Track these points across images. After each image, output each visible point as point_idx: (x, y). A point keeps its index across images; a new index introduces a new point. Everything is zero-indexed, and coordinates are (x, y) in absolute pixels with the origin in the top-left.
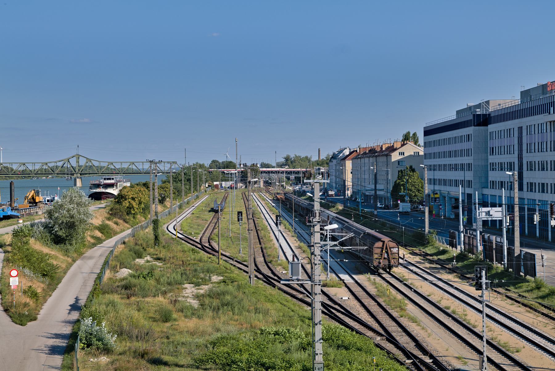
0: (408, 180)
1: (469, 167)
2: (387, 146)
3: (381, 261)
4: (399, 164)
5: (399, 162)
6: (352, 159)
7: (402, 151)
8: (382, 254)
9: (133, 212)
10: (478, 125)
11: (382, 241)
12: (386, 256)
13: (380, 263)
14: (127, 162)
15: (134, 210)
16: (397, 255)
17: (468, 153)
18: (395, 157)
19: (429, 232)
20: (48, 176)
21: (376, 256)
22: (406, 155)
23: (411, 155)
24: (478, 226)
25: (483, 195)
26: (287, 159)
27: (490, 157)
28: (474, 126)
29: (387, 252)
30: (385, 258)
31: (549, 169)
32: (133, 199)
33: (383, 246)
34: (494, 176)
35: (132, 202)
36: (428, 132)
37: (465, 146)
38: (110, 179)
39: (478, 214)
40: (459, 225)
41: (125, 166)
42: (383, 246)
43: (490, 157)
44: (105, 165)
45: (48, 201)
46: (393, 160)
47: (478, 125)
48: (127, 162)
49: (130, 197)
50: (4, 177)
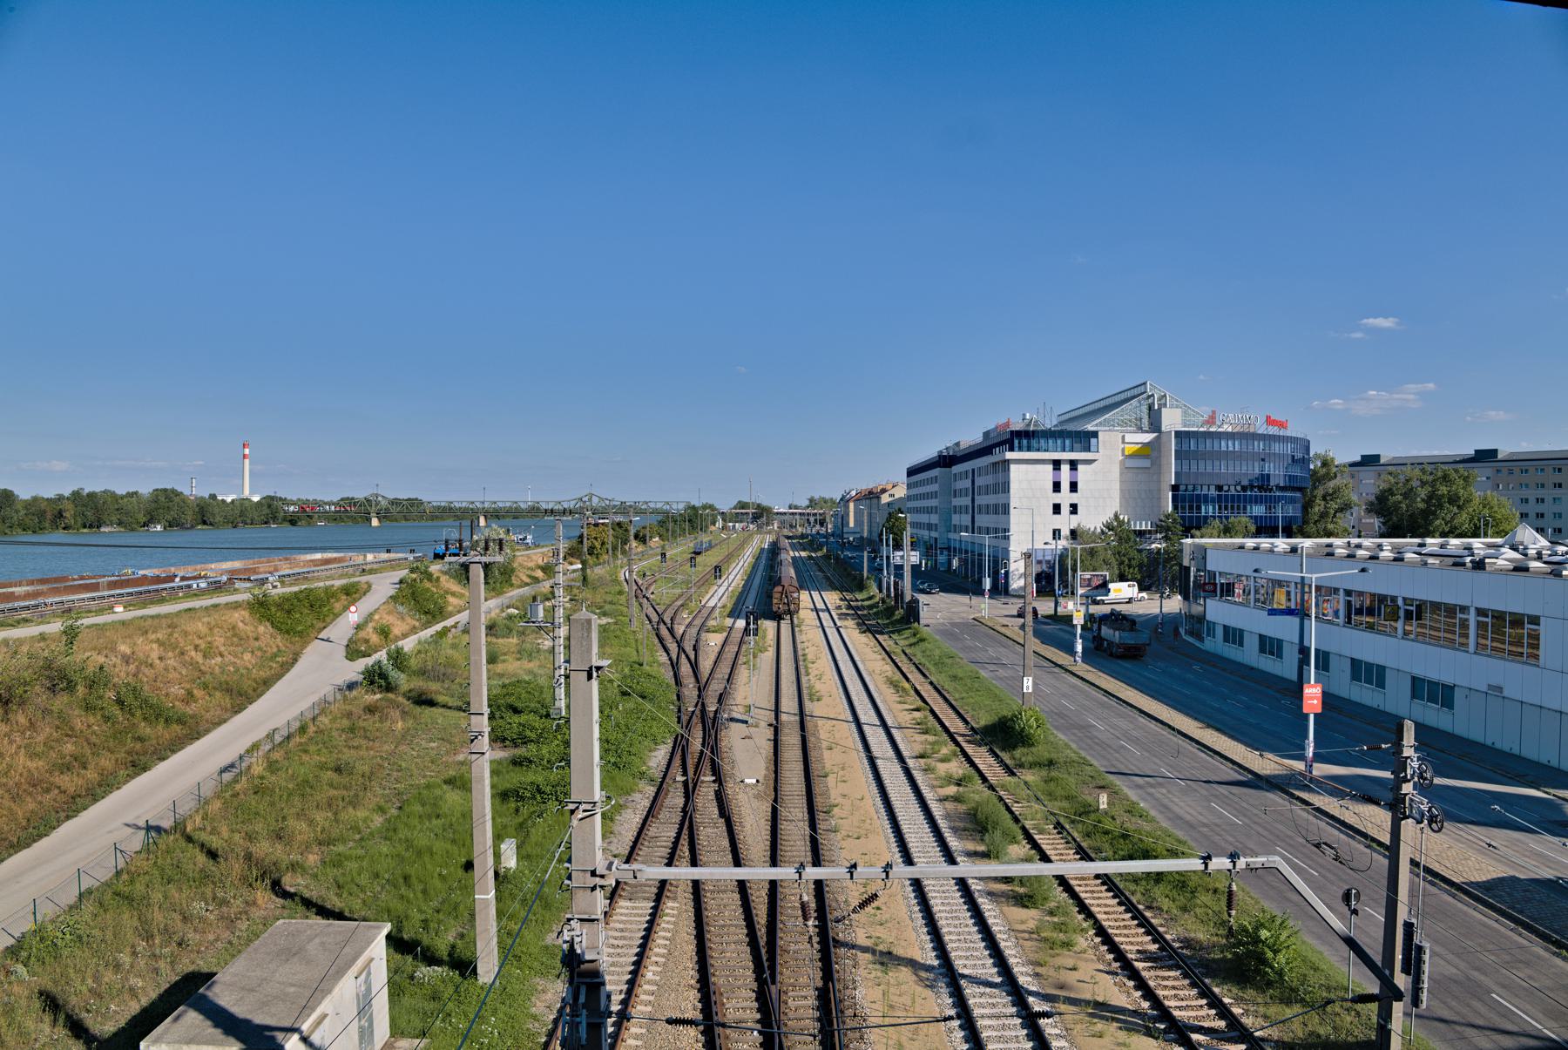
17: (934, 495)
18: (885, 499)
34: (956, 519)
36: (911, 472)
37: (934, 487)
41: (659, 506)
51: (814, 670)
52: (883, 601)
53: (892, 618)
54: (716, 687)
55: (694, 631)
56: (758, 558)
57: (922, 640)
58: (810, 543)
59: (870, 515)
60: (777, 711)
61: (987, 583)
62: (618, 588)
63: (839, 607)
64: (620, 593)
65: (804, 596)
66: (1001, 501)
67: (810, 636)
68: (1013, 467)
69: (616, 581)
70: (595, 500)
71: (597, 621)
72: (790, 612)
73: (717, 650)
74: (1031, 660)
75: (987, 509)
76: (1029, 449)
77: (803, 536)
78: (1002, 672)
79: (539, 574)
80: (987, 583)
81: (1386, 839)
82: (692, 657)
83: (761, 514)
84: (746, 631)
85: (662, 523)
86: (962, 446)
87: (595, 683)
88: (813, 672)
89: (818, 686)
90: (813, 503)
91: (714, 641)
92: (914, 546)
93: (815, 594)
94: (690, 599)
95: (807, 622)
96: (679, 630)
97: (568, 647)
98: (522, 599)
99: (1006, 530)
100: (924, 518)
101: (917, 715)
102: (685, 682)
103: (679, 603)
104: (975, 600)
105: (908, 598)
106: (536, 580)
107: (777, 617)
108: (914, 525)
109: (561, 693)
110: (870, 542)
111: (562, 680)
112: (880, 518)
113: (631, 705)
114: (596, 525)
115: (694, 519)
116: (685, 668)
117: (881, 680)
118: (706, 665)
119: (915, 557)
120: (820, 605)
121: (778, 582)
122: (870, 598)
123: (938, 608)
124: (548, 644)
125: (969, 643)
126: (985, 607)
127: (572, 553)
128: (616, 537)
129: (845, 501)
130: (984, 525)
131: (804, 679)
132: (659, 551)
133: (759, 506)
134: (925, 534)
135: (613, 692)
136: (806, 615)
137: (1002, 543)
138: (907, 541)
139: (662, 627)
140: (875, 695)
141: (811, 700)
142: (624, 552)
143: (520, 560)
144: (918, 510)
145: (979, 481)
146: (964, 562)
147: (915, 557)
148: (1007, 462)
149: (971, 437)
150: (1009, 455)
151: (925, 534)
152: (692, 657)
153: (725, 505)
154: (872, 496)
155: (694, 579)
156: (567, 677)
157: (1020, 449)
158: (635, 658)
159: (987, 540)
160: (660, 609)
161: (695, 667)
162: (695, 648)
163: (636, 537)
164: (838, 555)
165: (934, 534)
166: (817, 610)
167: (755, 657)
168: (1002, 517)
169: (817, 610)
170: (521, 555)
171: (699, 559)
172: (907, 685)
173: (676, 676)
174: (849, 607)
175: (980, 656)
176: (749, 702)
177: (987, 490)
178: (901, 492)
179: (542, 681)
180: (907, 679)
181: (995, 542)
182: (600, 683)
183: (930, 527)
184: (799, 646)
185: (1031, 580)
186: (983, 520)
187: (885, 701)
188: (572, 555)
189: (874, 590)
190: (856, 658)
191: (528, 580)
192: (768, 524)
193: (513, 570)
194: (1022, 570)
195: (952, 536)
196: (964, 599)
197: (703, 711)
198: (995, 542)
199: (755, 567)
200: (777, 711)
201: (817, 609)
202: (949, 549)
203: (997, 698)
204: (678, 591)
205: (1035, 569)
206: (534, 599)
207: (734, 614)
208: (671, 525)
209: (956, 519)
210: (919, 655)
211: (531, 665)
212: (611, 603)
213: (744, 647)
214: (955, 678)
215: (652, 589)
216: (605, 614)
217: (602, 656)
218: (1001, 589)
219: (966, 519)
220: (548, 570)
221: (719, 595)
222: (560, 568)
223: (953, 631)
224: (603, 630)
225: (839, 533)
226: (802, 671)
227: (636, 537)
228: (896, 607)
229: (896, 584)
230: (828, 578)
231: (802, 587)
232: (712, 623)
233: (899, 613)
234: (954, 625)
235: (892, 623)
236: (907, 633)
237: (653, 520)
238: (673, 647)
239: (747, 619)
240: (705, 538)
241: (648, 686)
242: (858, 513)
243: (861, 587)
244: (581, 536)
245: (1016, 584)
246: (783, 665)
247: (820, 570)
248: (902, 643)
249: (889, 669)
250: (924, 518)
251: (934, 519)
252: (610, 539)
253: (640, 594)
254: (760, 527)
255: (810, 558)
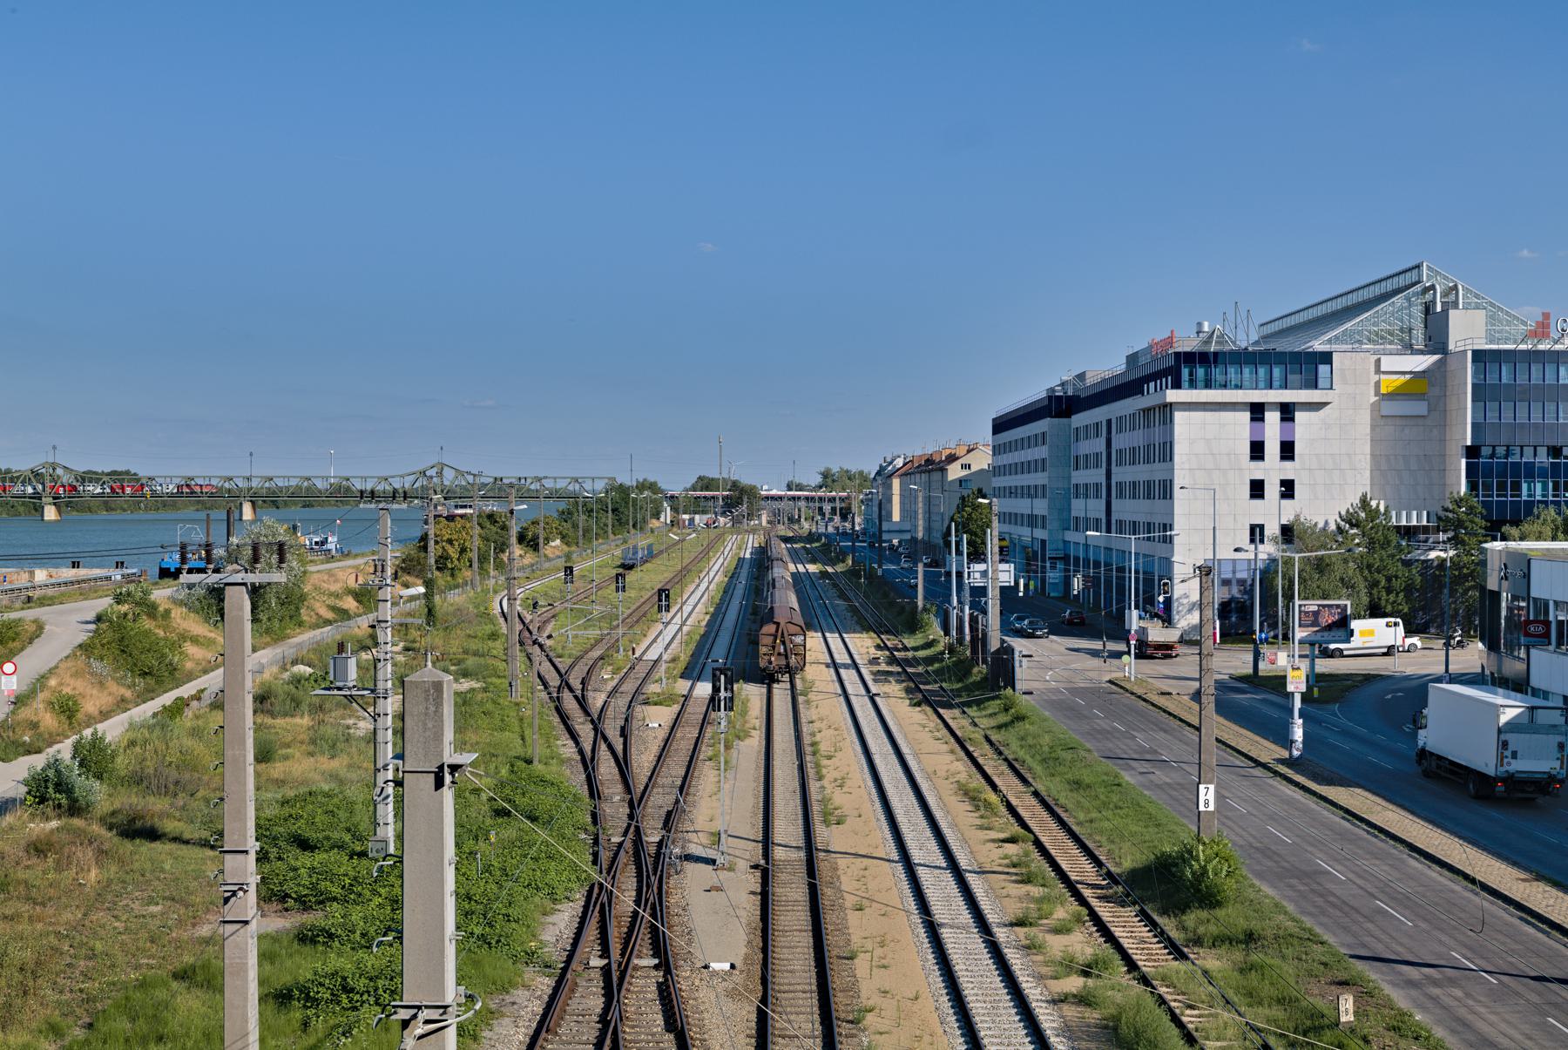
17: (1039, 465)
18: (955, 472)
19: (925, 609)
21: (763, 650)
22: (974, 469)
24: (967, 593)
27: (1074, 474)
29: (783, 643)
32: (450, 542)
34: (1078, 507)
35: (448, 547)
36: (1000, 426)
40: (950, 595)
41: (561, 484)
43: (1074, 474)
44: (293, 482)
47: (1057, 416)
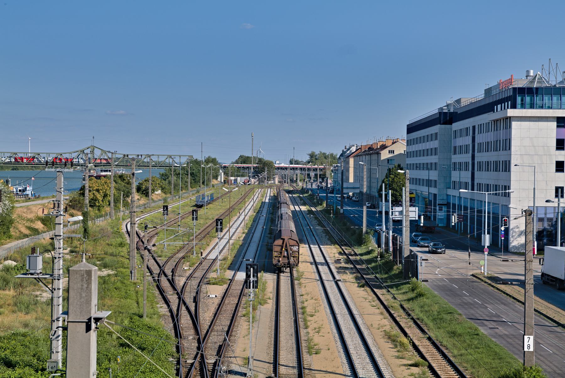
0: (393, 179)
1: (488, 165)
2: (381, 143)
3: (280, 259)
4: (388, 163)
5: (388, 160)
6: (354, 157)
7: (392, 150)
8: (281, 253)
9: (97, 204)
10: (445, 123)
11: (282, 239)
12: (286, 255)
13: (279, 261)
14: (164, 155)
15: (99, 202)
16: (297, 253)
17: (434, 152)
18: (385, 155)
19: (367, 233)
20: (76, 168)
21: (275, 254)
23: (401, 154)
25: (447, 195)
26: (312, 156)
27: (453, 156)
28: (441, 124)
29: (287, 250)
30: (284, 257)
31: (501, 170)
32: (98, 190)
33: (283, 243)
34: (455, 176)
35: (96, 193)
36: (411, 129)
37: (434, 144)
38: (107, 171)
39: (391, 214)
41: (162, 159)
42: (283, 243)
43: (453, 156)
45: (20, 191)
46: (382, 159)
48: (164, 155)
49: (95, 189)
50: (30, 168)
51: (312, 323)
52: (382, 256)
53: (391, 273)
54: (215, 339)
55: (194, 283)
56: (259, 212)
57: (420, 295)
58: (311, 198)
59: (370, 171)
60: (276, 364)
61: (487, 240)
62: (119, 240)
63: (338, 261)
64: (121, 245)
65: (304, 249)
66: (502, 159)
67: (309, 289)
68: (514, 124)
69: (118, 233)
70: (97, 153)
71: (97, 273)
72: (290, 266)
73: (217, 301)
74: (532, 318)
75: (487, 167)
76: (532, 106)
77: (303, 191)
78: (501, 330)
79: (39, 225)
80: (487, 240)
81: (324, 261)
82: (192, 309)
83: (262, 169)
84: (246, 283)
85: (164, 177)
86: (463, 104)
87: (93, 334)
88: (312, 325)
89: (317, 339)
90: (313, 158)
91: (215, 292)
92: (413, 202)
93: (315, 248)
94: (191, 251)
95: (306, 275)
96: (180, 282)
97: (66, 299)
98: (20, 251)
99: (507, 187)
100: (423, 174)
101: (415, 370)
102: (184, 333)
103: (180, 255)
104: (475, 256)
105: (406, 253)
106: (36, 232)
107: (277, 270)
108: (414, 181)
109: (58, 345)
110: (370, 197)
111: (60, 332)
112: (380, 174)
113: (130, 357)
114: (98, 177)
115: (196, 173)
116: (185, 320)
117: (379, 334)
118: (205, 317)
119: (413, 213)
120: (319, 259)
121: (279, 235)
122: (369, 253)
123: (437, 266)
124: (47, 295)
125: (469, 299)
126: (485, 264)
127: (74, 205)
128: (118, 189)
129: (345, 156)
130: (484, 182)
131: (302, 332)
132: (161, 203)
133: (260, 161)
134: (424, 190)
135: (113, 341)
136: (305, 268)
137: (502, 200)
138: (406, 197)
139: (163, 278)
140: (373, 349)
141: (310, 353)
142: (126, 205)
143: (18, 211)
144: (417, 167)
145: (480, 138)
146: (463, 218)
147: (413, 213)
148: (508, 120)
149: (473, 95)
150: (511, 112)
151: (424, 190)
152: (192, 309)
153: (227, 159)
154: (372, 152)
155: (196, 231)
156: (65, 329)
157: (523, 106)
158: (135, 309)
159: (487, 197)
160: (161, 261)
161: (195, 319)
162: (195, 300)
163: (139, 189)
164: (339, 211)
165: (433, 190)
166: (316, 264)
167: (254, 309)
168: (502, 174)
169: (316, 264)
170: (20, 207)
171: (201, 212)
172: (405, 340)
173: (176, 328)
174: (348, 261)
175: (479, 313)
176: (248, 354)
177: (487, 147)
178: (401, 148)
179: (40, 334)
180: (406, 334)
181: (495, 199)
182: (99, 336)
183: (429, 183)
184: (298, 299)
185: (532, 237)
186: (482, 177)
187: (382, 356)
188: (73, 207)
189: (373, 244)
190: (355, 312)
191: (27, 232)
192: (269, 178)
193: (11, 222)
194: (523, 228)
195: (451, 192)
196: (462, 255)
197: (202, 363)
198: (495, 199)
199: (255, 220)
200: (276, 364)
201: (316, 261)
202: (448, 205)
203: (497, 356)
204: (179, 243)
205: (537, 227)
206: (33, 250)
207: (234, 266)
208: (173, 179)
209: (455, 176)
210: (417, 310)
211: (28, 317)
212: (112, 255)
213: (244, 300)
214: (453, 334)
215: (154, 241)
216: (105, 266)
217: (101, 307)
218: (500, 246)
219: (466, 176)
220: (48, 221)
221: (221, 248)
222: (61, 220)
223: (453, 288)
224: (103, 281)
225: (338, 189)
226: (301, 324)
227: (139, 189)
228: (394, 262)
229: (394, 239)
230: (327, 232)
231: (301, 241)
232: (212, 275)
233: (398, 268)
234: (452, 280)
235: (391, 278)
236: (405, 288)
237: (157, 172)
238: (173, 299)
239: (247, 271)
240: (207, 192)
241: (151, 338)
242: (357, 168)
243: (360, 242)
244: (83, 188)
245: (516, 241)
246: (282, 318)
247: (320, 224)
248: (400, 297)
249: (387, 323)
250: (423, 174)
251: (434, 175)
252: (112, 192)
253: (142, 246)
254: (261, 181)
255: (310, 212)
